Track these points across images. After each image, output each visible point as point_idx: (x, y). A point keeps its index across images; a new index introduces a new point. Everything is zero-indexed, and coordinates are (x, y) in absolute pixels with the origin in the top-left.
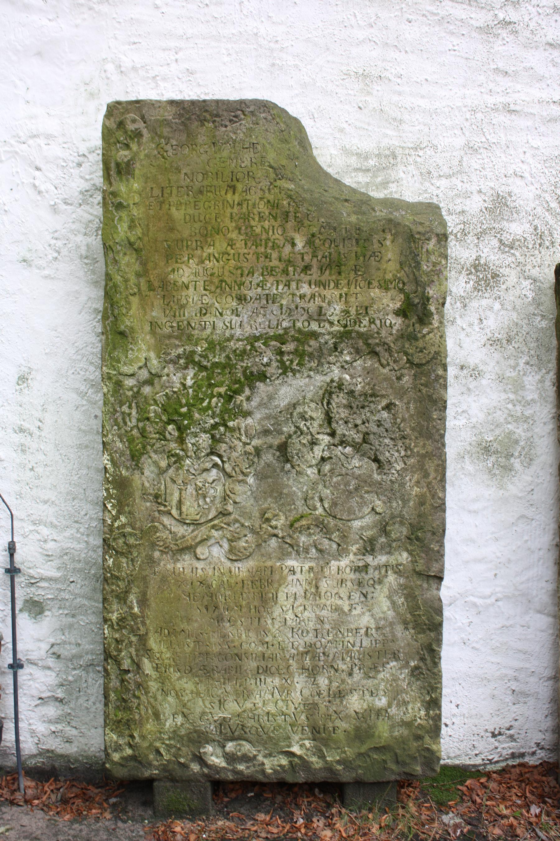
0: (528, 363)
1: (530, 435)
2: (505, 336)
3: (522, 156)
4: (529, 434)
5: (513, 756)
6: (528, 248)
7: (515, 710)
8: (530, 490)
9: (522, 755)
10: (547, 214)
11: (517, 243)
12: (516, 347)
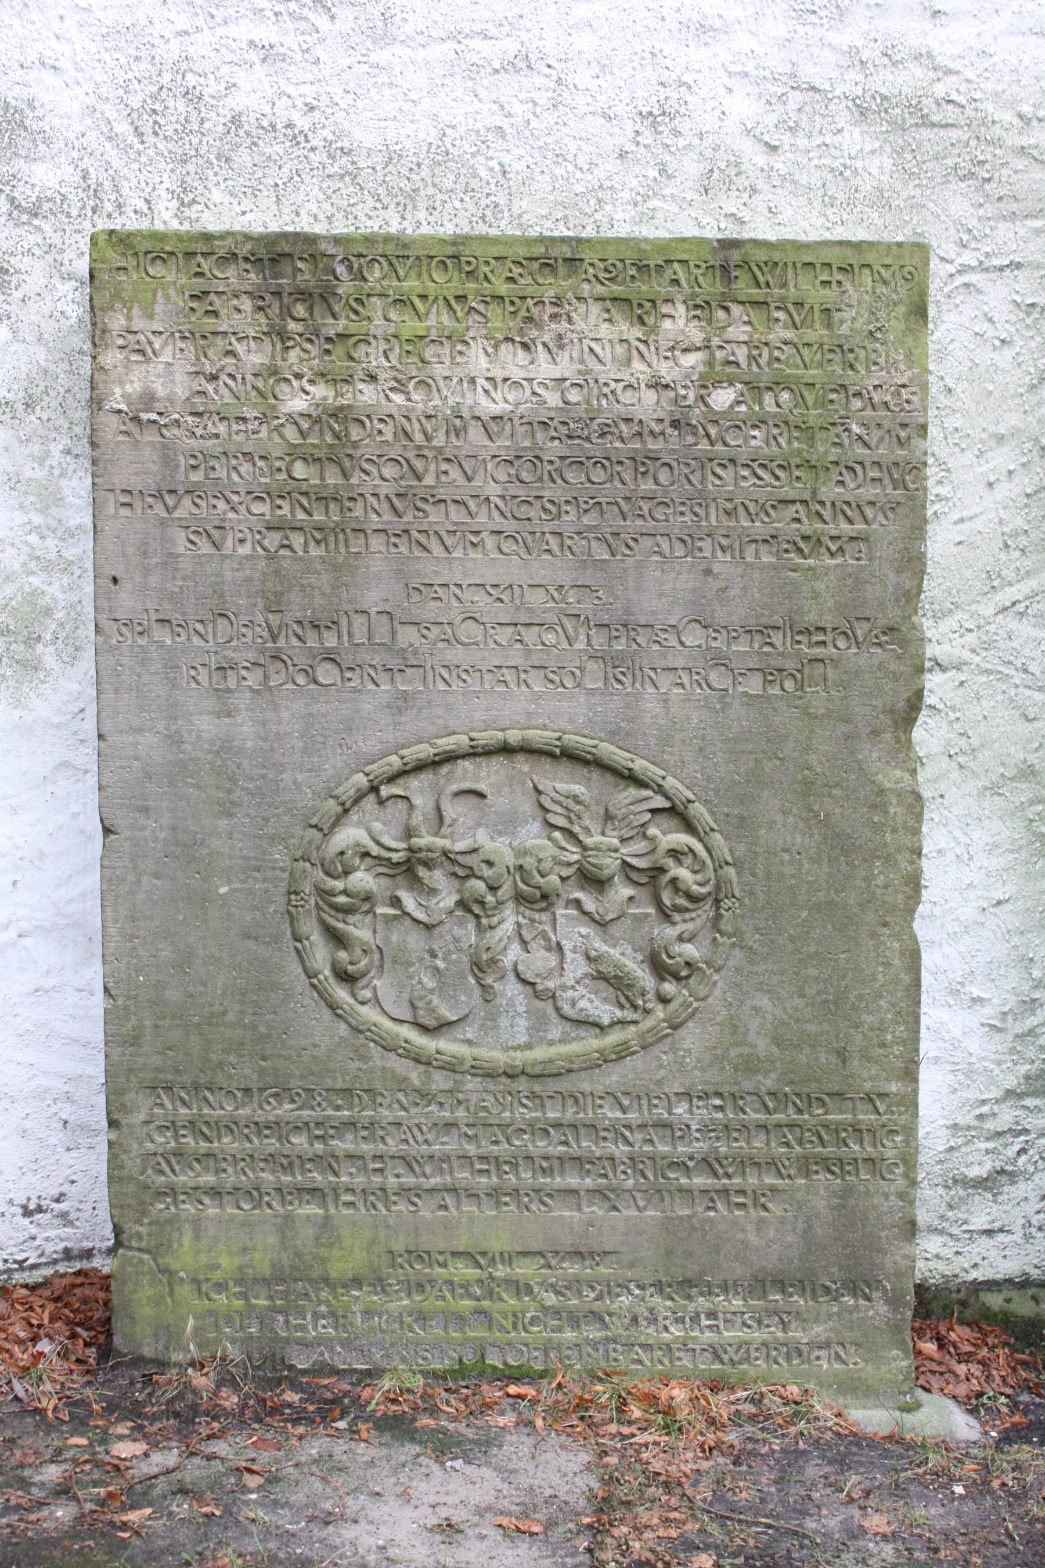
0: (68, 452)
1: (76, 599)
2: (21, 395)
3: (55, 24)
4: (74, 597)
5: (68, 1254)
6: (68, 215)
7: (71, 1162)
8: (76, 710)
9: (88, 1254)
10: (108, 145)
11: (46, 206)
12: (45, 418)
